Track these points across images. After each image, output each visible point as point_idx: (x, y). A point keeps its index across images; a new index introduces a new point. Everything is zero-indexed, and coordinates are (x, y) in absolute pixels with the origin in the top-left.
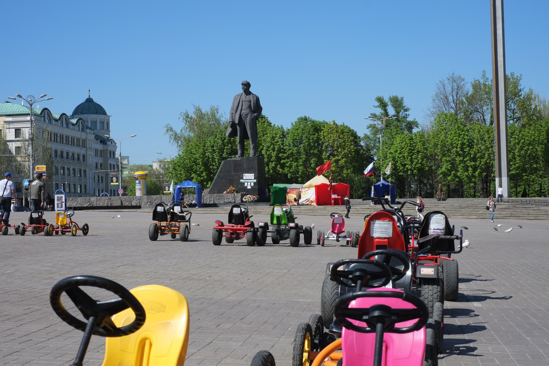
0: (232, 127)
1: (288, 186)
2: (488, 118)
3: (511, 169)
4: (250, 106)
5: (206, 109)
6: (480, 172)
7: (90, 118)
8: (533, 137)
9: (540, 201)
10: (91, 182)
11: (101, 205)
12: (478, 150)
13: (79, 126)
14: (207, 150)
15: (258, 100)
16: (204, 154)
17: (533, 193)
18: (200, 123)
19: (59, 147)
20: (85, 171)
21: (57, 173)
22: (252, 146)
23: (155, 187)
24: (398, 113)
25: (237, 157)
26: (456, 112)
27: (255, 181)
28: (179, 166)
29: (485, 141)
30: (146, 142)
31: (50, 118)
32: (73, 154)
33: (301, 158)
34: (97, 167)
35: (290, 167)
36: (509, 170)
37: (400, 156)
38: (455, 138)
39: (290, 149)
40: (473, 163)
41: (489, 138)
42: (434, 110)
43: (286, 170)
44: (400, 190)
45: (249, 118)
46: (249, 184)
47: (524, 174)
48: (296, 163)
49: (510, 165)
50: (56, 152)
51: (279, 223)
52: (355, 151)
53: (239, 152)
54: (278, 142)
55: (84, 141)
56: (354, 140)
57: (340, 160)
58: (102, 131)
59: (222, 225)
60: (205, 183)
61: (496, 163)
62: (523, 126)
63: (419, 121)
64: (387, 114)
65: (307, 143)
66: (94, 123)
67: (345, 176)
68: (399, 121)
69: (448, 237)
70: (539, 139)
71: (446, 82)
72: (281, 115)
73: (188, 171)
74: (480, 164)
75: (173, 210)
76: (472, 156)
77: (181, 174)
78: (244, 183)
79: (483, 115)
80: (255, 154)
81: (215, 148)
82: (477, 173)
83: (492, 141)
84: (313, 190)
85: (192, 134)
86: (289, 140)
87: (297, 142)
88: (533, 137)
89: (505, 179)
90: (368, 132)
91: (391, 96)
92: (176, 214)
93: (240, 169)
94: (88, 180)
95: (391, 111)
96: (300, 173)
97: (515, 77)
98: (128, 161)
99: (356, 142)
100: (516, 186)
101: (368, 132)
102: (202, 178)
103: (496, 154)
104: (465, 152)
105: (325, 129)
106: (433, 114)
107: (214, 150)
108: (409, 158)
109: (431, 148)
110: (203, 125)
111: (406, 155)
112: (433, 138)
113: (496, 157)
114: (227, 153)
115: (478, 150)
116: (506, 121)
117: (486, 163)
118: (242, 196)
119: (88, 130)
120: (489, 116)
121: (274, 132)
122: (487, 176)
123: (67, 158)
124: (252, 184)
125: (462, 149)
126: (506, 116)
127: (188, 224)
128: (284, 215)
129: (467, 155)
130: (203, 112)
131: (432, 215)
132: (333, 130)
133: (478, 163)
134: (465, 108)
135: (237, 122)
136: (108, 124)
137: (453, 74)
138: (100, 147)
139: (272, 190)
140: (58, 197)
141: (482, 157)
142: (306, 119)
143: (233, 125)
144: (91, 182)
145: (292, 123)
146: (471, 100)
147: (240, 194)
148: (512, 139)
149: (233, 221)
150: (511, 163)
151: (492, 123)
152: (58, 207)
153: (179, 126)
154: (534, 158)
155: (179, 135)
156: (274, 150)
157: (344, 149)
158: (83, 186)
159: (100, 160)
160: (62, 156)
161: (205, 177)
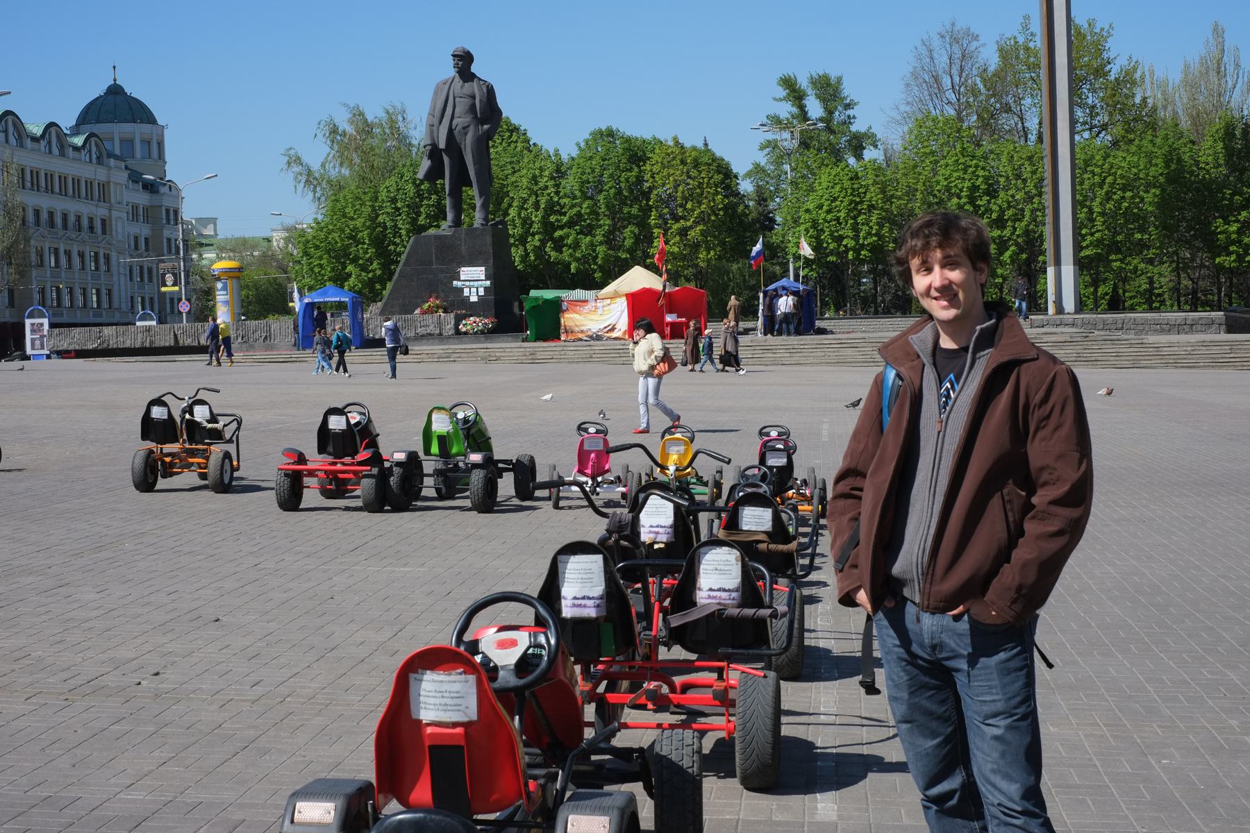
0: (430, 157)
1: (563, 294)
2: (1032, 123)
3: (1084, 244)
4: (472, 108)
5: (374, 113)
6: (1014, 253)
7: (118, 131)
8: (1135, 170)
9: (1145, 322)
10: (122, 283)
11: (128, 344)
12: (1009, 203)
13: (90, 151)
14: (381, 207)
15: (490, 92)
16: (374, 217)
17: (1134, 297)
18: (363, 143)
19: (45, 202)
20: (107, 257)
21: (41, 264)
22: (478, 202)
23: (277, 290)
24: (831, 113)
25: (445, 226)
26: (959, 113)
27: (488, 283)
28: (317, 247)
29: (1025, 181)
30: (246, 184)
31: (20, 135)
32: (78, 218)
33: (600, 226)
34: (136, 248)
35: (576, 245)
36: (1078, 248)
37: (829, 217)
38: (955, 174)
39: (573, 206)
40: (996, 233)
41: (1034, 172)
42: (908, 108)
43: (566, 255)
44: (837, 292)
45: (476, 129)
46: (474, 290)
47: (1113, 257)
48: (588, 238)
49: (1080, 234)
50: (37, 213)
51: (445, 453)
52: (725, 208)
53: (450, 216)
54: (547, 187)
55: (104, 187)
56: (722, 183)
57: (691, 227)
58: (148, 162)
59: (301, 459)
60: (378, 286)
61: (1048, 231)
62: (1115, 144)
63: (879, 132)
64: (803, 115)
65: (612, 191)
66: (128, 143)
67: (702, 264)
68: (832, 132)
69: (749, 612)
70: (1147, 175)
71: (936, 42)
72: (555, 119)
73: (337, 258)
74: (1013, 234)
75: (192, 414)
76: (994, 216)
77: (321, 266)
78: (461, 290)
79: (1022, 119)
80: (486, 219)
81: (399, 205)
82: (1008, 254)
83: (1042, 180)
84: (622, 304)
85: (346, 172)
86: (570, 183)
87: (591, 188)
88: (1135, 170)
89: (1068, 270)
90: (762, 159)
91: (814, 75)
92: (199, 424)
93: (453, 257)
94: (115, 278)
95: (815, 108)
96: (599, 261)
97: (1097, 30)
98: (215, 230)
99: (727, 188)
100: (1095, 283)
101: (762, 159)
102: (370, 275)
103: (1049, 211)
104: (979, 206)
105: (656, 158)
106: (906, 117)
107: (397, 209)
108: (851, 221)
109: (899, 198)
110: (372, 149)
111: (842, 214)
112: (905, 175)
113: (1049, 219)
114: (428, 216)
115: (1009, 203)
116: (1073, 133)
117: (1027, 232)
118: (458, 320)
119: (112, 162)
120: (1036, 121)
121: (538, 165)
122: (1028, 262)
123: (65, 227)
124: (481, 292)
125: (972, 200)
126: (1073, 122)
127: (232, 448)
128: (456, 431)
129: (983, 214)
130: (370, 118)
131: (702, 550)
132: (674, 158)
133: (1007, 232)
134: (980, 106)
135: (442, 145)
136: (160, 145)
137: (953, 24)
138: (143, 199)
139: (527, 306)
140: (33, 325)
141: (1017, 218)
142: (611, 134)
143: (434, 153)
144: (122, 283)
145: (578, 144)
146: (996, 82)
147: (452, 315)
148: (1086, 176)
149: (330, 449)
150: (1084, 232)
151: (1040, 139)
152: (33, 348)
153: (317, 153)
154: (1137, 218)
155: (317, 175)
156: (536, 206)
157: (700, 203)
158: (104, 292)
159: (144, 230)
160: (52, 224)
161: (379, 272)
